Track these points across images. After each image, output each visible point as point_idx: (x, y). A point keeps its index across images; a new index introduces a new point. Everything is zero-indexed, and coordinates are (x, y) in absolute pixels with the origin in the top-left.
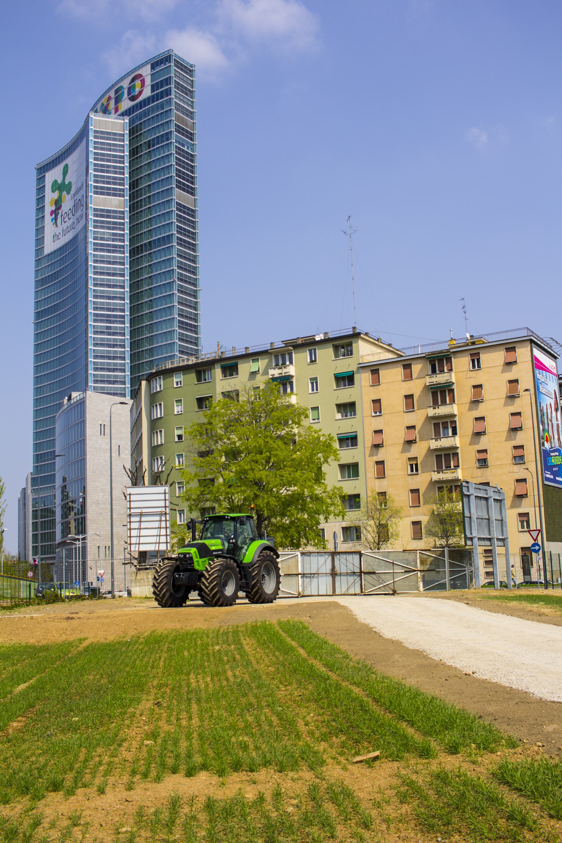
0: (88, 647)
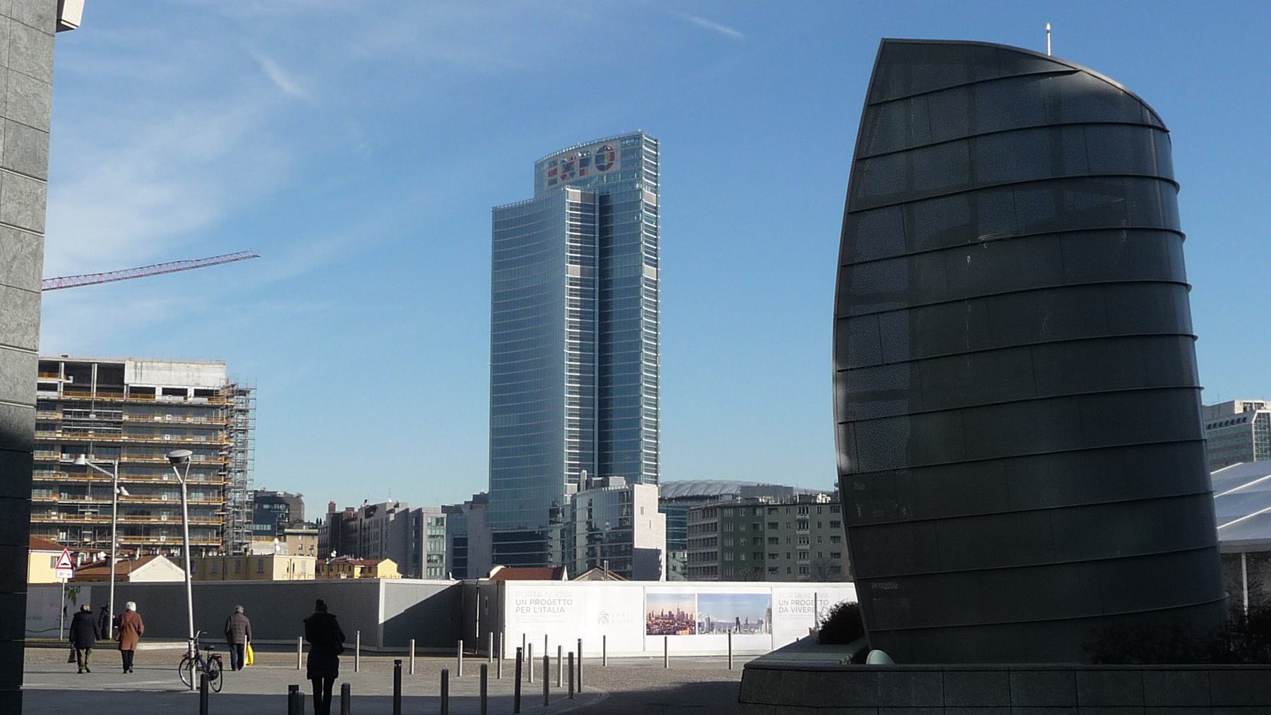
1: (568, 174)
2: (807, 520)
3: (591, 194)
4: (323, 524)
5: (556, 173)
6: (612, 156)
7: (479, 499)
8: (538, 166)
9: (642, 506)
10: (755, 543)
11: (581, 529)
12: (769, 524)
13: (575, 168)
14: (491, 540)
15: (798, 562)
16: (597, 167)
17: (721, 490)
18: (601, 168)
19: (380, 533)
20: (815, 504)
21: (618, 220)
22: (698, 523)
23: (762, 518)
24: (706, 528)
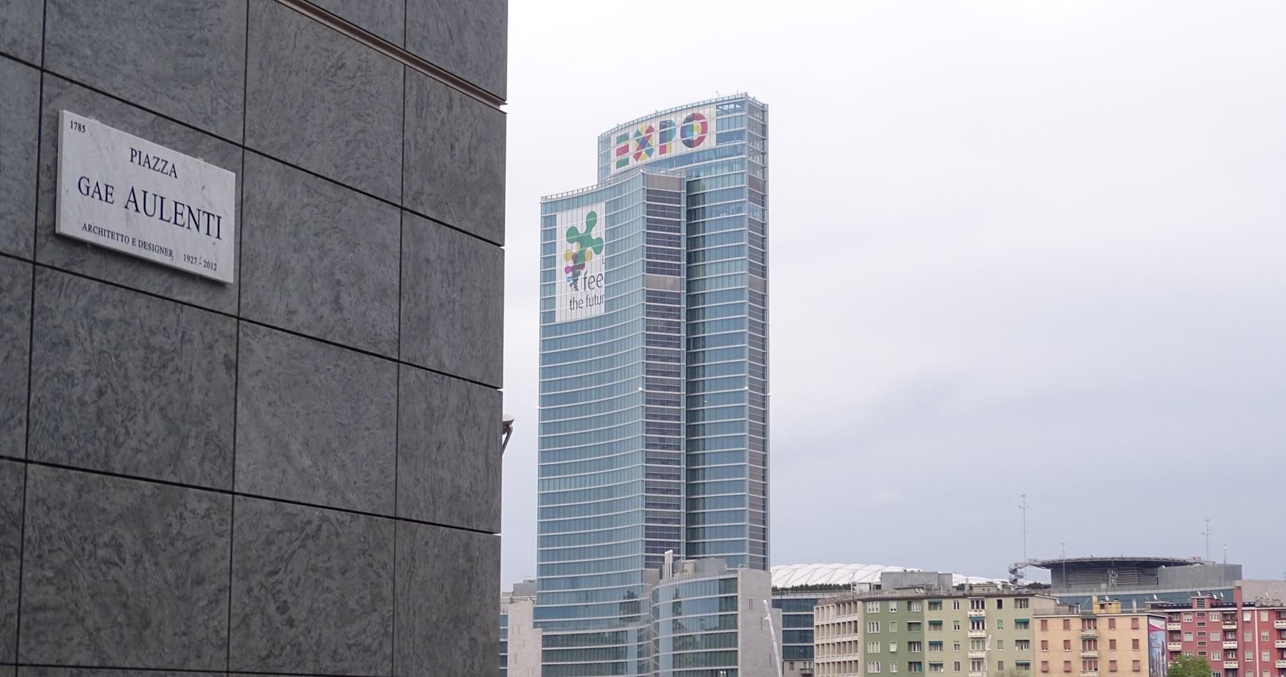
0: (288, 278)
8: (604, 141)
18: (689, 144)
23: (921, 614)
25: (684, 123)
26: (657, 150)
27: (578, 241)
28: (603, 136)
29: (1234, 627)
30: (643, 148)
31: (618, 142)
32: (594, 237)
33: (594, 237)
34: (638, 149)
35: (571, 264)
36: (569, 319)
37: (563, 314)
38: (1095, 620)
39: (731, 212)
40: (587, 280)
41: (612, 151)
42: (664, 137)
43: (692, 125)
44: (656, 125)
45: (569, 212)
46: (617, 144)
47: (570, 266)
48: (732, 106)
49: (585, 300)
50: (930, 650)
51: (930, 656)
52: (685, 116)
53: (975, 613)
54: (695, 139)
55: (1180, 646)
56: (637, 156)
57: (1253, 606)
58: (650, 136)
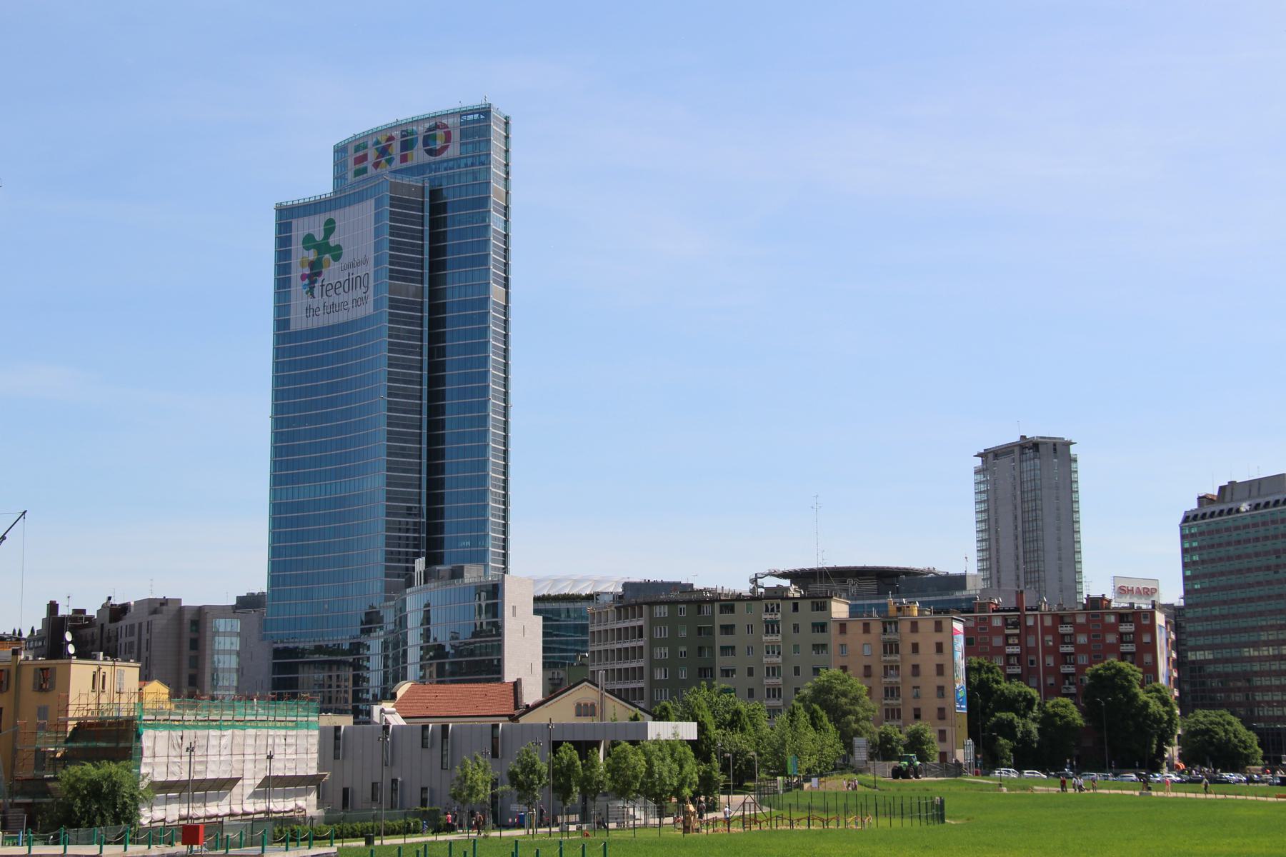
1: (383, 160)
2: (777, 622)
3: (416, 187)
4: (36, 634)
5: (366, 160)
6: (448, 137)
7: (248, 603)
8: (340, 150)
9: (513, 604)
10: (700, 655)
11: (414, 638)
12: (722, 627)
13: (394, 153)
14: (271, 658)
15: (766, 681)
16: (425, 150)
17: (573, 586)
18: (431, 152)
19: (136, 643)
20: (788, 598)
21: (455, 223)
22: (608, 627)
23: (711, 619)
24: (620, 634)
25: (426, 132)
26: (398, 159)
27: (314, 248)
28: (340, 145)
29: (1017, 631)
30: (383, 157)
31: (356, 151)
32: (332, 244)
33: (332, 244)
34: (378, 158)
35: (307, 271)
36: (304, 327)
37: (299, 322)
38: (896, 623)
39: (475, 221)
40: (325, 287)
41: (349, 160)
42: (407, 145)
43: (435, 134)
44: (397, 134)
45: (306, 219)
46: (355, 152)
47: (307, 273)
48: (476, 116)
49: (322, 308)
50: (722, 655)
51: (721, 662)
52: (427, 125)
53: (770, 616)
54: (438, 148)
55: (1019, 650)
56: (376, 165)
57: (1036, 610)
58: (391, 144)
